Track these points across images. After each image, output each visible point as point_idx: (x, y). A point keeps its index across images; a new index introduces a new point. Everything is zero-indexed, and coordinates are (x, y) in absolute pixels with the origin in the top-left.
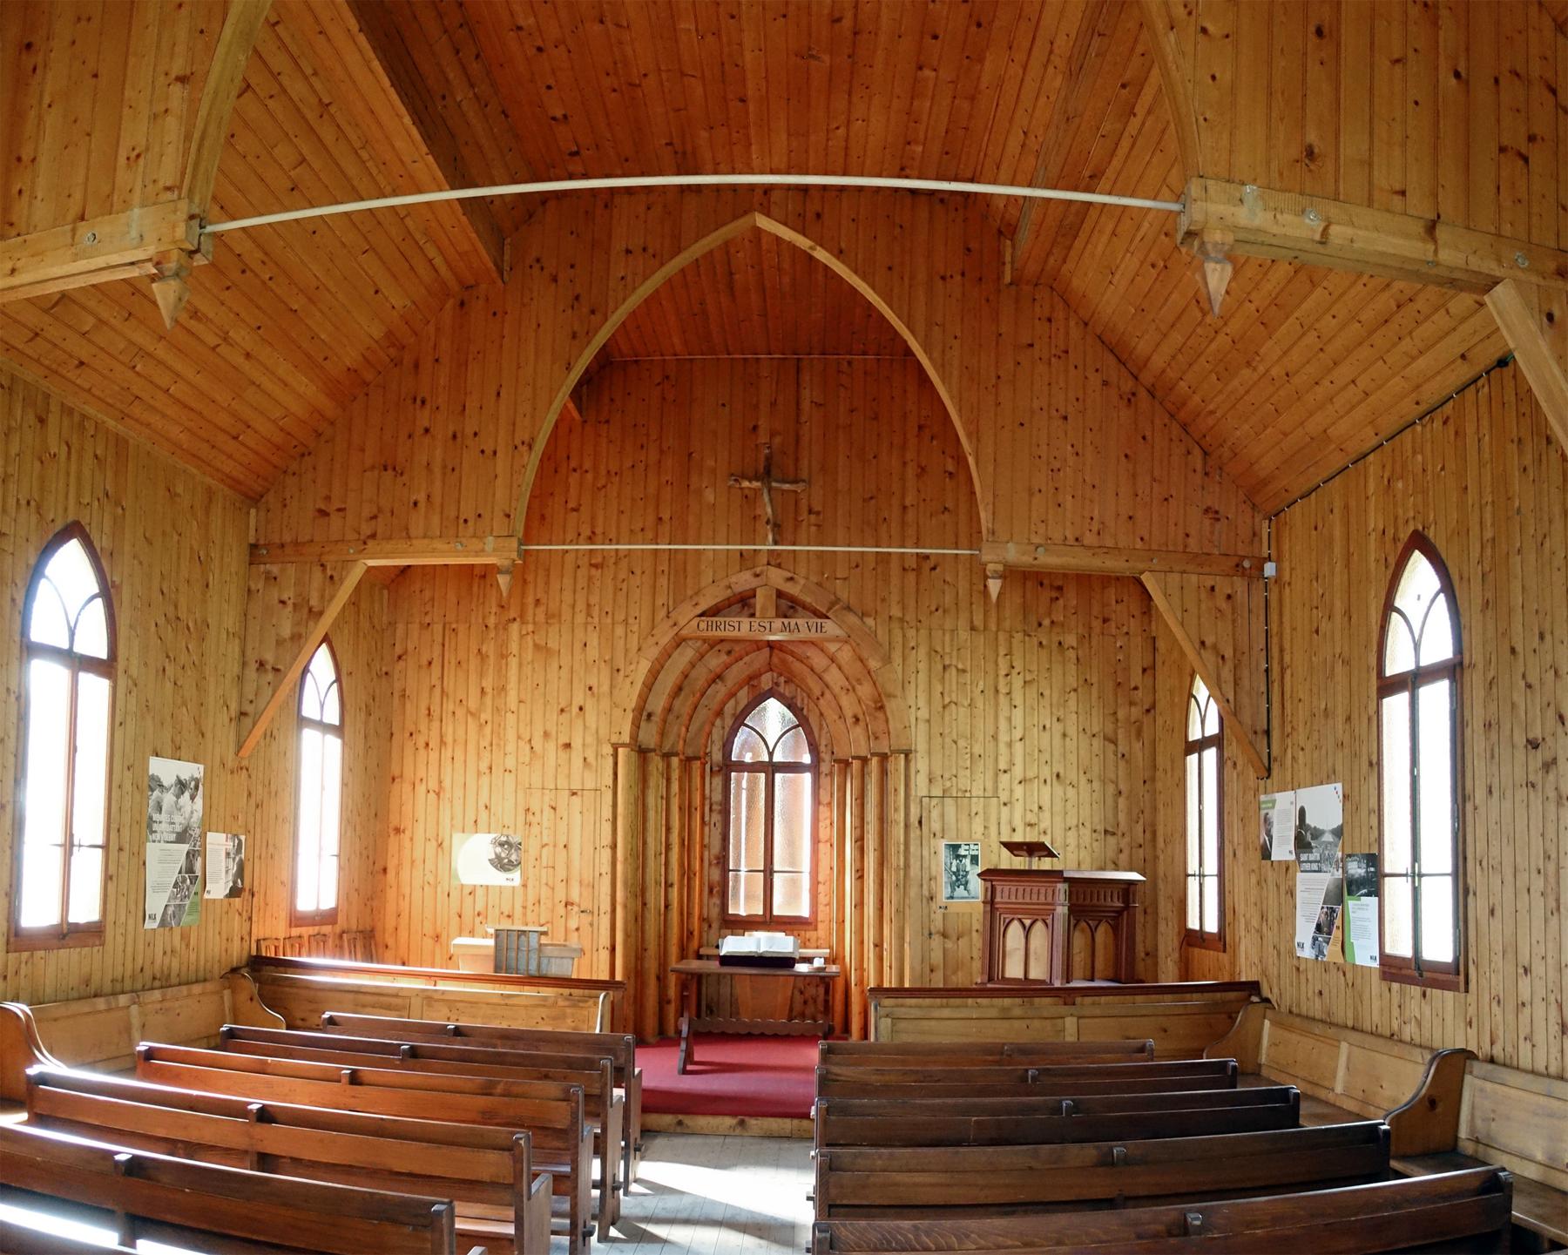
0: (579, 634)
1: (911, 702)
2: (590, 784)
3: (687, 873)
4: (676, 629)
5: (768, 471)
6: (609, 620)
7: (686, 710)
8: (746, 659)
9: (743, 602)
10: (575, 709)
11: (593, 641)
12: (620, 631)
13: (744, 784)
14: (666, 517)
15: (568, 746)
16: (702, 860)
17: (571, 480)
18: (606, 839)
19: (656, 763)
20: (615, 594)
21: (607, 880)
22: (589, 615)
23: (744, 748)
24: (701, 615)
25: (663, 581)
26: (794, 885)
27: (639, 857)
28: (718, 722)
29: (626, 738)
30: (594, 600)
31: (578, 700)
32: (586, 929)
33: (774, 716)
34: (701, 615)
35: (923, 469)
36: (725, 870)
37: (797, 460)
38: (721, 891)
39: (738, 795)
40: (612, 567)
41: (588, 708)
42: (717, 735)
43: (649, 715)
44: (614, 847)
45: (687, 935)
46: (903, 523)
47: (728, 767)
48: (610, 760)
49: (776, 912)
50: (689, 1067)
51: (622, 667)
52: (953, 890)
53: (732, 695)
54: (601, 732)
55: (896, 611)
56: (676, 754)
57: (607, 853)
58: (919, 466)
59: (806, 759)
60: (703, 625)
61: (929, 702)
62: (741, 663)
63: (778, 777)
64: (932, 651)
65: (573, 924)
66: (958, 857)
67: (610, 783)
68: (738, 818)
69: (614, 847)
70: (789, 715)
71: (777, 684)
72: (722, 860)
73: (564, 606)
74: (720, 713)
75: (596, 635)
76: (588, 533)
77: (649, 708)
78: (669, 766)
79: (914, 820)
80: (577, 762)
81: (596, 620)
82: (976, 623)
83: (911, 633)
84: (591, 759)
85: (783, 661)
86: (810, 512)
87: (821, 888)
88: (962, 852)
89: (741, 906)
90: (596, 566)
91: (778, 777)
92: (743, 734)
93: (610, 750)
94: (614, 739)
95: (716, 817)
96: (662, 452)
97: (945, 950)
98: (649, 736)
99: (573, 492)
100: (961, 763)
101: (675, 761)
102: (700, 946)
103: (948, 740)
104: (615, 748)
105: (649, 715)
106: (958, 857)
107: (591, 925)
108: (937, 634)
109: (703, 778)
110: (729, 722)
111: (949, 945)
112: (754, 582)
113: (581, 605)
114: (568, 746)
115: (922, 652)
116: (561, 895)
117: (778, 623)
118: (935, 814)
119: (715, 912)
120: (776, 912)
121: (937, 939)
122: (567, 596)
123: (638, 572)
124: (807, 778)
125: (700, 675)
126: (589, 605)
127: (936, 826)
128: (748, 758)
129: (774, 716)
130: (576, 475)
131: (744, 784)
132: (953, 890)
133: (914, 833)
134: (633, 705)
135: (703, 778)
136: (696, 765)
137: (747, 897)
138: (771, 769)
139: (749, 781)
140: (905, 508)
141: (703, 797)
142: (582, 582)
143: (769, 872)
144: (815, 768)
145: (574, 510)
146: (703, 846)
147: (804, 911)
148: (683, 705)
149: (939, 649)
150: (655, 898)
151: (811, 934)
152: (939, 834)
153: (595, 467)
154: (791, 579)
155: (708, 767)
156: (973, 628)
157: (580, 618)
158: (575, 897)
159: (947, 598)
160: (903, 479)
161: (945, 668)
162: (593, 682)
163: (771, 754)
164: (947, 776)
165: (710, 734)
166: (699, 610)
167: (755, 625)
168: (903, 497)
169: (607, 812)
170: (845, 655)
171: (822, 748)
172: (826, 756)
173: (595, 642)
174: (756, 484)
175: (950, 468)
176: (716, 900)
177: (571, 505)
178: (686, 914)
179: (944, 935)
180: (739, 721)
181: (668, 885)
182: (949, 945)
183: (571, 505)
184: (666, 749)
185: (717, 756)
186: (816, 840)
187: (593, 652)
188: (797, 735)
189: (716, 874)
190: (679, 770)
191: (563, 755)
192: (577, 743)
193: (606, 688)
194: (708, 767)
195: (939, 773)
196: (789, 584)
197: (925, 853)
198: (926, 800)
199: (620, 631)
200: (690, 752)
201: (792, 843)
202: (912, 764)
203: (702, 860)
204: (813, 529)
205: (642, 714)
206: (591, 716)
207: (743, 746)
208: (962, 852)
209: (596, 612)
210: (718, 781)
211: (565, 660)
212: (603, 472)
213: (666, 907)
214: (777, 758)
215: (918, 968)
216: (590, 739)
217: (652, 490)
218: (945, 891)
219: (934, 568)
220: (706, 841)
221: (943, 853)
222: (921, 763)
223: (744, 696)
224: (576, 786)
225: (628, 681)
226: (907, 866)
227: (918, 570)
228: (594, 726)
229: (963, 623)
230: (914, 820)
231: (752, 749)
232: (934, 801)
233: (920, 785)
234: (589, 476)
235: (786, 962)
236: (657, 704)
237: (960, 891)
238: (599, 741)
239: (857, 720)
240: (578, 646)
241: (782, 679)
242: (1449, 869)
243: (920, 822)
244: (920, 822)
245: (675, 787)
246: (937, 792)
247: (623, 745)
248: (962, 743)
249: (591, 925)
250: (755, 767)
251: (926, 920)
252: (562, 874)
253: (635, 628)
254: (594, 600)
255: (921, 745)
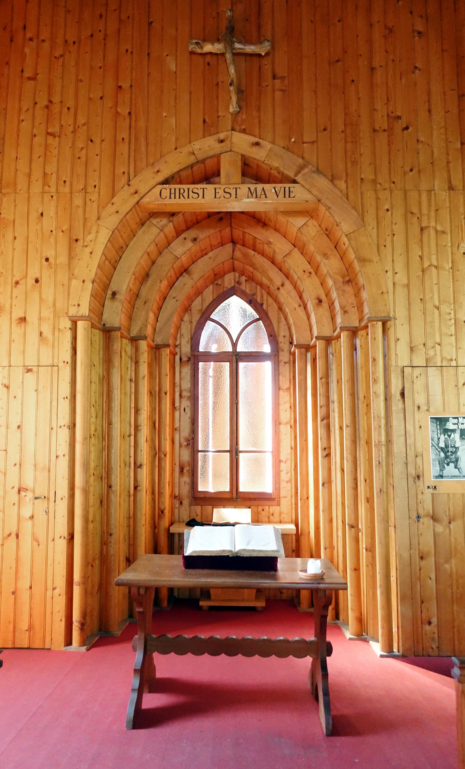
0: (36, 206)
1: (389, 267)
2: (46, 360)
3: (157, 454)
4: (137, 197)
5: (231, 30)
6: (67, 190)
7: (155, 297)
8: (210, 254)
9: (207, 174)
10: (31, 281)
11: (50, 211)
12: (78, 201)
13: (211, 372)
14: (125, 85)
15: (23, 320)
16: (173, 442)
17: (27, 50)
18: (65, 419)
19: (122, 346)
20: (73, 163)
21: (64, 464)
22: (45, 183)
23: (211, 339)
24: (166, 182)
25: (123, 149)
26: (257, 464)
27: (104, 438)
28: (186, 318)
29: (85, 310)
30: (51, 168)
31: (34, 273)
32: (41, 518)
33: (235, 311)
34: (166, 182)
35: (391, 30)
36: (194, 452)
37: (259, 27)
38: (191, 470)
39: (206, 382)
40: (71, 136)
41: (44, 280)
42: (186, 330)
43: (114, 294)
44: (73, 427)
45: (157, 514)
46: (372, 86)
47: (196, 357)
48: (68, 335)
49: (242, 489)
50: (152, 701)
51: (80, 237)
52: (442, 469)
53: (199, 293)
54: (58, 305)
55: (368, 174)
56: (145, 338)
57: (65, 434)
58: (386, 27)
59: (267, 348)
60: (166, 193)
61: (408, 265)
62: (206, 257)
63: (242, 365)
64: (408, 213)
65: (26, 512)
66: (446, 431)
67: (67, 357)
68: (206, 404)
69: (73, 427)
70: (250, 310)
71: (239, 283)
72: (192, 442)
73: (19, 174)
74: (187, 309)
75: (53, 203)
76: (46, 103)
77: (113, 287)
78: (137, 349)
79: (395, 390)
80: (33, 337)
81: (53, 189)
82: (454, 183)
83: (384, 195)
84: (47, 332)
85: (245, 255)
86: (274, 77)
87: (283, 466)
88: (450, 426)
89: (213, 481)
90: (53, 135)
91: (242, 365)
92: (209, 326)
93: (69, 324)
94: (73, 311)
95: (186, 403)
96: (120, 21)
97: (435, 535)
98: (114, 315)
99: (29, 61)
100: (444, 330)
101: (143, 345)
102: (172, 524)
103: (429, 306)
104: (74, 323)
105: (114, 294)
106: (446, 431)
107: (47, 513)
108: (413, 195)
109: (173, 367)
110: (196, 317)
111: (440, 528)
112: (217, 148)
113: (37, 174)
114: (23, 320)
115: (399, 213)
116: (13, 480)
117: (244, 189)
118: (419, 385)
119: (185, 490)
120: (242, 489)
121: (427, 522)
122: (23, 166)
123: (97, 141)
124: (267, 366)
125: (166, 265)
126: (45, 174)
127: (420, 399)
128: (214, 349)
129: (235, 311)
130: (34, 44)
131: (211, 372)
132: (442, 469)
133: (396, 404)
134: (92, 275)
135: (173, 367)
136: (166, 352)
137: (215, 476)
138: (235, 358)
139: (215, 371)
140: (373, 69)
141: (173, 384)
142: (38, 151)
143: (234, 452)
144: (275, 356)
145: (29, 79)
146: (174, 429)
147: (267, 487)
148: (152, 291)
149: (415, 210)
150: (120, 479)
151: (274, 509)
152: (424, 408)
153: (53, 39)
154: (257, 144)
155: (177, 358)
156: (451, 188)
157: (36, 188)
158: (29, 482)
159: (422, 159)
160: (370, 41)
161: (422, 229)
162: (50, 254)
163: (234, 345)
164: (430, 344)
165: (178, 328)
166: (161, 177)
167: (220, 192)
168: (371, 58)
169: (65, 390)
170: (310, 231)
171: (281, 339)
172: (284, 345)
173: (52, 213)
174: (217, 48)
175: (420, 28)
176: (186, 479)
177: (28, 73)
178: (155, 493)
179: (434, 518)
180: (205, 316)
181: (138, 466)
182: (440, 528)
183: (28, 73)
184: (134, 332)
185: (186, 349)
186: (277, 423)
187: (49, 223)
188: (258, 328)
189: (186, 455)
190: (141, 349)
191: (17, 330)
192: (32, 318)
193: (63, 259)
194: (177, 358)
195: (422, 341)
196: (255, 149)
197: (410, 427)
198: (408, 371)
199: (78, 201)
200: (159, 340)
201: (254, 426)
202: (391, 332)
203: (173, 442)
204: (278, 94)
205: (103, 292)
206: (48, 291)
207: (209, 338)
208: (450, 426)
209: (53, 181)
210: (187, 370)
211: (20, 231)
212: (60, 40)
213: (136, 488)
214: (240, 348)
215: (406, 555)
216: (47, 313)
217: (111, 58)
218: (434, 470)
219: (407, 128)
220: (177, 425)
221: (431, 429)
222: (400, 330)
223: (209, 294)
224: (31, 362)
225: (88, 250)
226: (389, 441)
227: (390, 131)
228: (51, 299)
229: (439, 184)
230: (395, 390)
231: (218, 341)
232: (417, 372)
233: (401, 355)
234: (46, 45)
235: (266, 564)
236: (124, 282)
237: (450, 469)
238: (56, 315)
239: (320, 301)
240: (34, 215)
241: (243, 278)
242: (241, 455)
243: (403, 394)
244: (403, 394)
245: (144, 369)
246: (419, 360)
247: (82, 318)
248: (445, 308)
249: (47, 513)
250: (219, 357)
251: (413, 502)
252: (14, 457)
253: (94, 197)
254: (51, 168)
255: (400, 313)
